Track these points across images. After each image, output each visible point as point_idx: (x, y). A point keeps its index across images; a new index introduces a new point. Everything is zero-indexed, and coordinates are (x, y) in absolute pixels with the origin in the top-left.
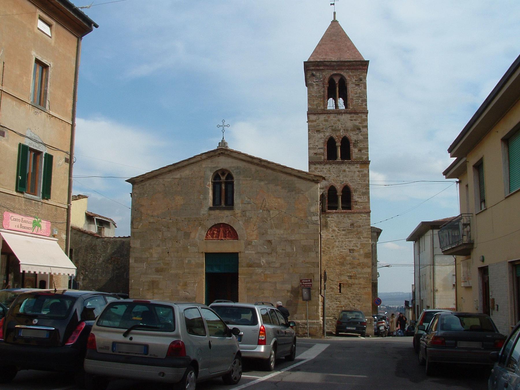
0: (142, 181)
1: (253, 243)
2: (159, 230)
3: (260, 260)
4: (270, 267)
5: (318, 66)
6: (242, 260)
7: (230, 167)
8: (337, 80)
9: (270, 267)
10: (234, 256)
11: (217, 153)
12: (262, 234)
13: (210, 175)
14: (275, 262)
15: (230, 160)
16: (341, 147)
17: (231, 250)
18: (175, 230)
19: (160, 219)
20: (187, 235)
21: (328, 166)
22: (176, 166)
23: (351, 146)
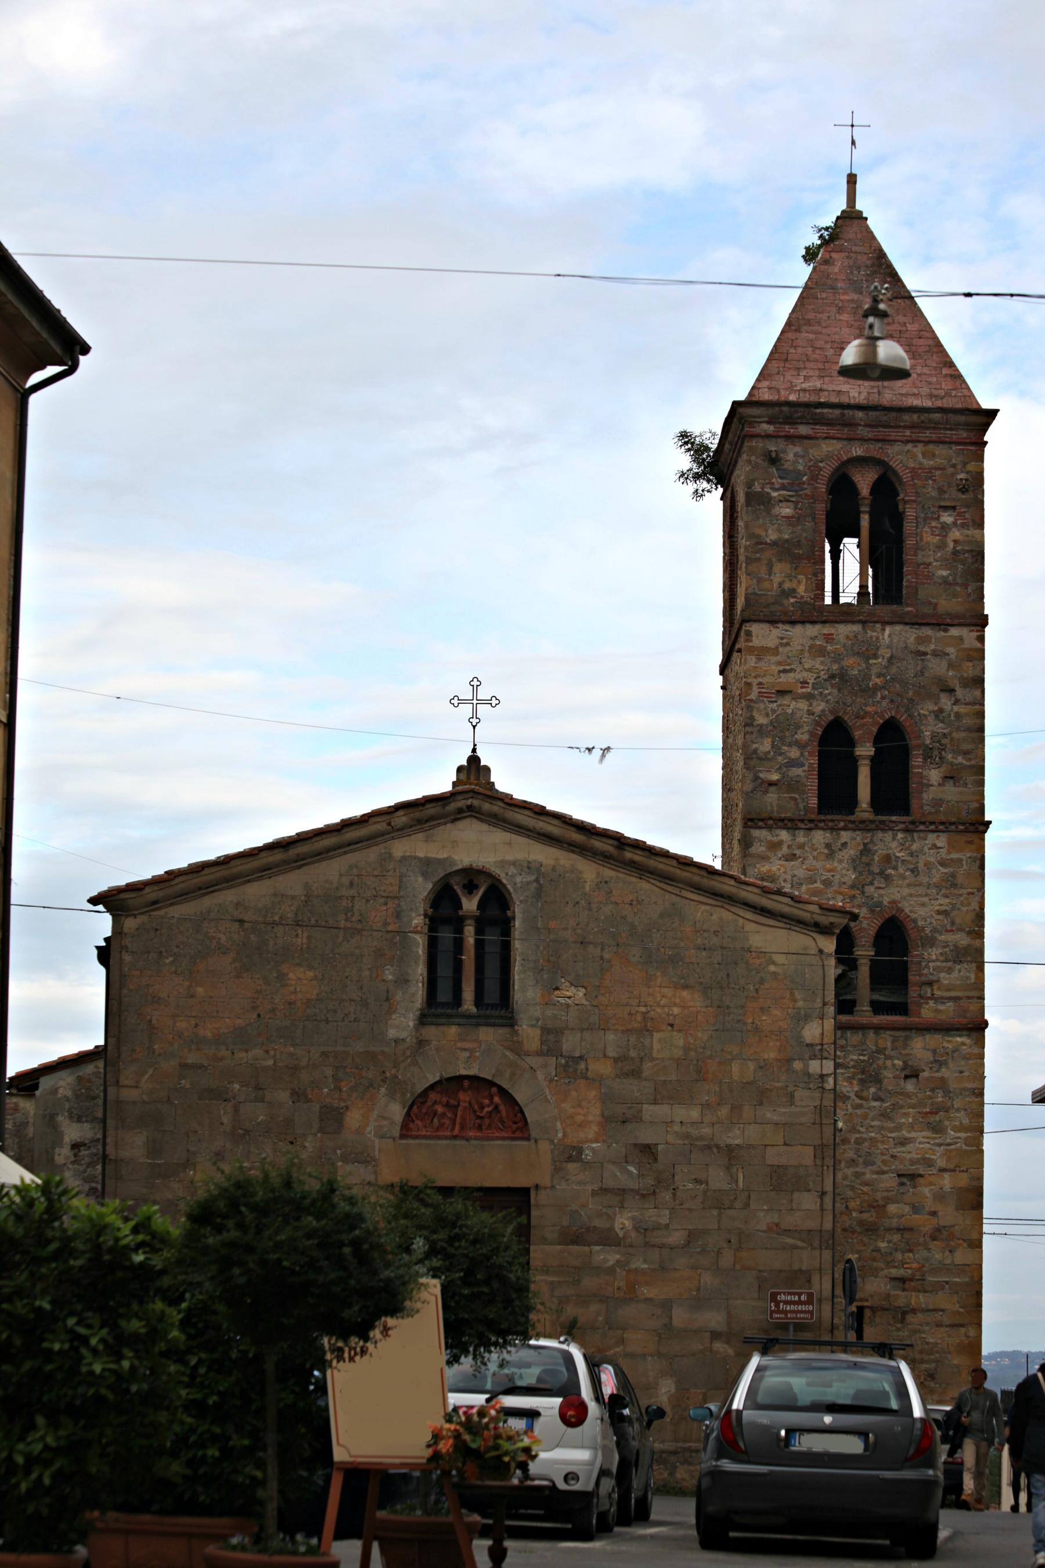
0: (155, 903)
1: (588, 1155)
2: (218, 1095)
3: (611, 1218)
4: (647, 1244)
5: (791, 421)
6: (544, 1214)
7: (503, 864)
8: (864, 482)
9: (647, 1244)
10: (519, 1198)
11: (453, 806)
12: (618, 1119)
13: (422, 888)
14: (667, 1226)
15: (499, 836)
16: (876, 762)
17: (498, 1177)
18: (283, 1096)
19: (223, 1052)
20: (332, 1118)
21: (820, 837)
22: (293, 852)
23: (916, 760)
